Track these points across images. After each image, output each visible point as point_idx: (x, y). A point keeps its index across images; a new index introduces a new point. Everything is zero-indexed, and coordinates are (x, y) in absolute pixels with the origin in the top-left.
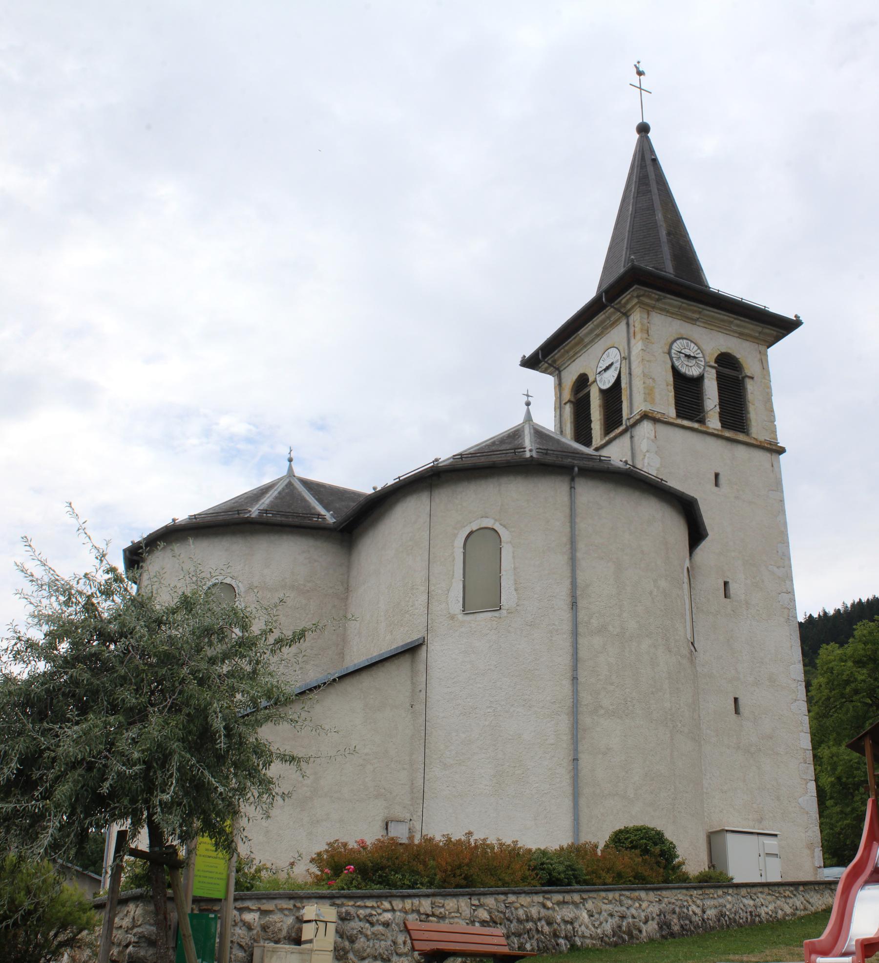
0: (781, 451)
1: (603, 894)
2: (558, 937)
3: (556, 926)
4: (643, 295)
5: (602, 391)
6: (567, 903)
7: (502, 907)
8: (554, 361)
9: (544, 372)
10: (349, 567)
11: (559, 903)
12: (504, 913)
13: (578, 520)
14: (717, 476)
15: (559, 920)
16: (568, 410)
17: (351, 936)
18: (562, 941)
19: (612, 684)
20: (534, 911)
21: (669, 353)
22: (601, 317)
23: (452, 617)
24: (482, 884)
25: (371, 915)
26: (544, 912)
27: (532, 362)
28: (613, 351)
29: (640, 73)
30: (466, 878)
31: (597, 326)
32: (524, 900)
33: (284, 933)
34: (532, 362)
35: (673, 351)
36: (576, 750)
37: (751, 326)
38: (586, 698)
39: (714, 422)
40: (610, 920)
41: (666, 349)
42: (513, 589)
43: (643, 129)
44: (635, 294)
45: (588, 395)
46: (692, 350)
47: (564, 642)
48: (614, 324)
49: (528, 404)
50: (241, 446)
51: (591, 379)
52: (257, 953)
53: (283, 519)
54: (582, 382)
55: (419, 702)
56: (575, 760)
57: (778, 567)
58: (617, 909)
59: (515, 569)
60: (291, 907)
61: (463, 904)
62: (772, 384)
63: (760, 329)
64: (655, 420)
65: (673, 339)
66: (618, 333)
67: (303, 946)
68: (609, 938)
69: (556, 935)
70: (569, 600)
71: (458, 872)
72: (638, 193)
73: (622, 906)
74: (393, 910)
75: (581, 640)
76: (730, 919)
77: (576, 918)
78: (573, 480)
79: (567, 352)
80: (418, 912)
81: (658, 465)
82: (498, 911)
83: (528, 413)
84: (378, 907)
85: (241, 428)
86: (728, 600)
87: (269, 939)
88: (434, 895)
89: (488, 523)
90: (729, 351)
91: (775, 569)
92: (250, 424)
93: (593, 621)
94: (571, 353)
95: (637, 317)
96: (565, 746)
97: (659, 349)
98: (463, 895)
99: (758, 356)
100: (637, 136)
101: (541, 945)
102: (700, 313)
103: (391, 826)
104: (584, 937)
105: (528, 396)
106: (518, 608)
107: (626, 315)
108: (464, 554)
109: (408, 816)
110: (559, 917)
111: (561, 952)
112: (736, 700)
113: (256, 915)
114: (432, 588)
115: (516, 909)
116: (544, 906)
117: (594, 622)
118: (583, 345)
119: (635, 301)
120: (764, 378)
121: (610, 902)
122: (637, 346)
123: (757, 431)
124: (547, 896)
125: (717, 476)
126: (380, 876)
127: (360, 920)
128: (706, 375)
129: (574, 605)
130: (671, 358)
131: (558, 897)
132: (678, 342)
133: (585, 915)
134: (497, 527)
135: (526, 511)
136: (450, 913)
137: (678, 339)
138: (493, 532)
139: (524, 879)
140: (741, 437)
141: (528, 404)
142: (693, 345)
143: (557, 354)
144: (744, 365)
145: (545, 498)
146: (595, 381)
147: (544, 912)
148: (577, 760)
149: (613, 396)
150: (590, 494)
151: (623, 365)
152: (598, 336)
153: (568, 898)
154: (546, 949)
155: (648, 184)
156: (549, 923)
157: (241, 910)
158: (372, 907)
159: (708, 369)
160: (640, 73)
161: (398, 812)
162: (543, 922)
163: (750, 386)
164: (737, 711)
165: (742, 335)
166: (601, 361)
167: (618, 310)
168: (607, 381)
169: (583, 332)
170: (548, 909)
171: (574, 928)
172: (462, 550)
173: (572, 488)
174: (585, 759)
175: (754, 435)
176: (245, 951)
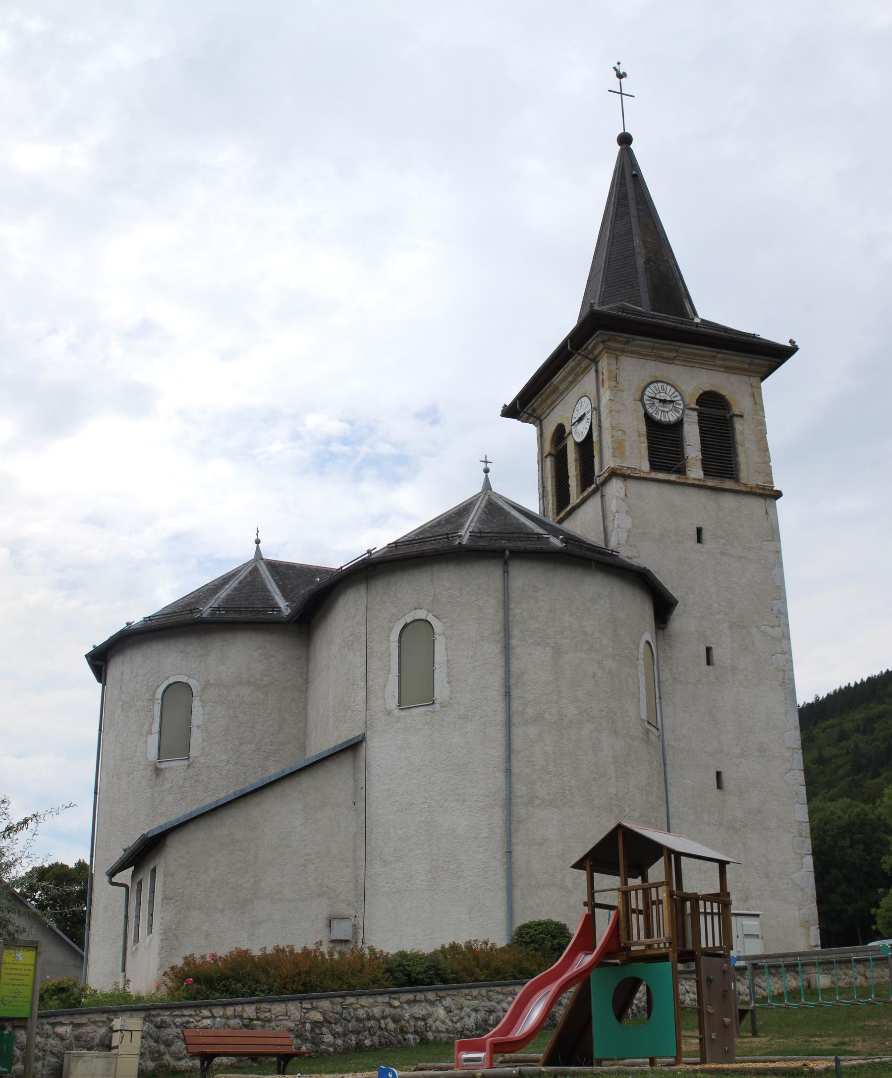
0: (778, 495)
1: (466, 991)
2: (407, 1033)
3: (403, 1023)
4: (609, 340)
5: (576, 444)
6: (419, 1001)
7: (338, 1008)
8: (534, 411)
9: (526, 421)
10: (308, 659)
11: (409, 1002)
12: (341, 1014)
13: (511, 606)
14: (699, 531)
15: (407, 1016)
16: (549, 462)
17: (167, 1041)
18: (411, 1036)
19: (549, 773)
20: (377, 1011)
21: (642, 400)
22: (571, 364)
23: (389, 713)
24: (321, 988)
25: (188, 1022)
26: (388, 1010)
27: (510, 412)
28: (585, 400)
29: (620, 76)
30: (304, 985)
31: (569, 373)
32: (364, 1001)
33: (97, 1041)
34: (510, 412)
35: (646, 397)
36: (509, 843)
37: (739, 358)
38: (520, 789)
39: (695, 472)
40: (473, 1014)
41: (638, 397)
42: (446, 681)
43: (625, 140)
44: (600, 339)
45: (565, 447)
46: (668, 393)
47: (497, 733)
48: (585, 370)
49: (486, 471)
50: (335, 448)
51: (567, 431)
52: (66, 1057)
53: (236, 615)
54: (560, 434)
55: (360, 800)
56: (509, 852)
57: (772, 627)
58: (483, 1004)
59: (448, 661)
60: (104, 1019)
61: (292, 1008)
62: (766, 419)
63: (749, 360)
64: (625, 477)
65: (646, 383)
66: (588, 381)
67: (113, 1051)
68: (471, 1032)
69: (403, 1031)
70: (503, 690)
71: (296, 979)
72: (616, 215)
73: (490, 1001)
74: (213, 1017)
75: (515, 731)
76: (638, 1007)
77: (430, 1015)
78: (506, 563)
79: (545, 400)
80: (241, 1017)
81: (629, 526)
82: (334, 1013)
83: (487, 480)
84: (197, 1015)
85: (335, 427)
86: (711, 667)
87: (83, 1047)
88: (259, 1002)
89: (421, 614)
90: (714, 389)
91: (769, 629)
92: (341, 421)
93: (528, 710)
94: (549, 402)
95: (604, 363)
96: (499, 839)
97: (629, 397)
98: (293, 1000)
99: (749, 389)
100: (618, 148)
101: (383, 1040)
102: (677, 351)
103: (335, 923)
104: (438, 1031)
105: (486, 462)
106: (451, 701)
107: (595, 361)
108: (400, 647)
109: (353, 913)
110: (407, 1015)
111: (411, 1046)
112: (719, 774)
113: (69, 1029)
114: (370, 683)
115: (356, 1009)
116: (391, 1005)
117: (530, 711)
118: (559, 394)
119: (601, 346)
120: (757, 414)
121: (475, 998)
122: (606, 396)
123: (748, 475)
124: (394, 996)
125: (699, 531)
126: (224, 986)
127: (177, 1027)
128: (685, 419)
129: (508, 694)
130: (644, 406)
131: (410, 997)
132: (651, 386)
133: (441, 1012)
134: (430, 618)
135: (458, 603)
136: (276, 1017)
137: (652, 383)
138: (425, 623)
139: (375, 982)
140: (728, 484)
141: (486, 471)
142: (669, 387)
143: (535, 403)
144: (732, 402)
145: (477, 586)
146: (570, 433)
147: (388, 1010)
148: (511, 852)
149: (586, 447)
150: (524, 577)
151: (594, 416)
152: (571, 383)
153: (420, 996)
154: (389, 1044)
155: (627, 206)
156: (396, 1020)
157: (54, 1025)
158: (191, 1016)
159: (687, 412)
160: (620, 76)
161: (342, 909)
162: (389, 1020)
163: (739, 426)
164: (719, 786)
165: (729, 369)
166: (576, 410)
167: (585, 357)
168: (579, 433)
169: (556, 379)
170: (395, 1007)
171: (426, 1024)
172: (397, 644)
173: (506, 572)
174: (519, 851)
175: (743, 481)
176: (58, 1057)
